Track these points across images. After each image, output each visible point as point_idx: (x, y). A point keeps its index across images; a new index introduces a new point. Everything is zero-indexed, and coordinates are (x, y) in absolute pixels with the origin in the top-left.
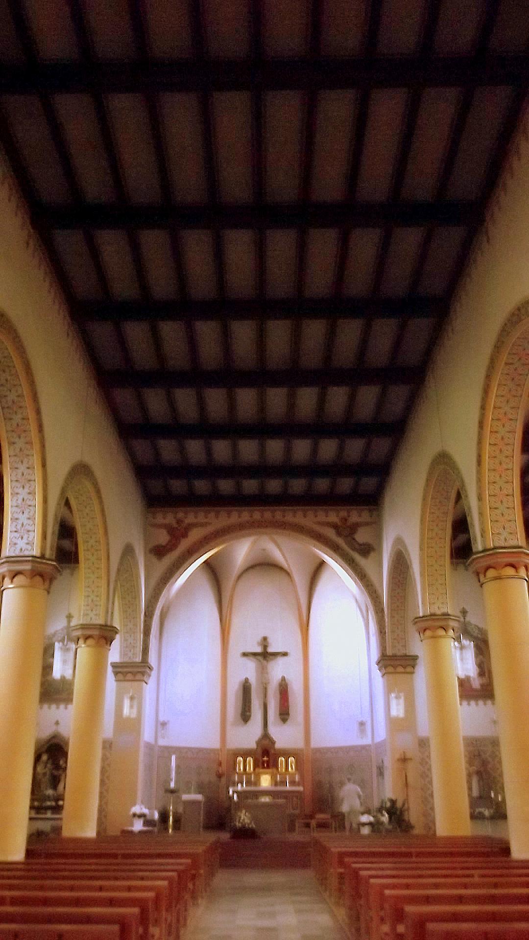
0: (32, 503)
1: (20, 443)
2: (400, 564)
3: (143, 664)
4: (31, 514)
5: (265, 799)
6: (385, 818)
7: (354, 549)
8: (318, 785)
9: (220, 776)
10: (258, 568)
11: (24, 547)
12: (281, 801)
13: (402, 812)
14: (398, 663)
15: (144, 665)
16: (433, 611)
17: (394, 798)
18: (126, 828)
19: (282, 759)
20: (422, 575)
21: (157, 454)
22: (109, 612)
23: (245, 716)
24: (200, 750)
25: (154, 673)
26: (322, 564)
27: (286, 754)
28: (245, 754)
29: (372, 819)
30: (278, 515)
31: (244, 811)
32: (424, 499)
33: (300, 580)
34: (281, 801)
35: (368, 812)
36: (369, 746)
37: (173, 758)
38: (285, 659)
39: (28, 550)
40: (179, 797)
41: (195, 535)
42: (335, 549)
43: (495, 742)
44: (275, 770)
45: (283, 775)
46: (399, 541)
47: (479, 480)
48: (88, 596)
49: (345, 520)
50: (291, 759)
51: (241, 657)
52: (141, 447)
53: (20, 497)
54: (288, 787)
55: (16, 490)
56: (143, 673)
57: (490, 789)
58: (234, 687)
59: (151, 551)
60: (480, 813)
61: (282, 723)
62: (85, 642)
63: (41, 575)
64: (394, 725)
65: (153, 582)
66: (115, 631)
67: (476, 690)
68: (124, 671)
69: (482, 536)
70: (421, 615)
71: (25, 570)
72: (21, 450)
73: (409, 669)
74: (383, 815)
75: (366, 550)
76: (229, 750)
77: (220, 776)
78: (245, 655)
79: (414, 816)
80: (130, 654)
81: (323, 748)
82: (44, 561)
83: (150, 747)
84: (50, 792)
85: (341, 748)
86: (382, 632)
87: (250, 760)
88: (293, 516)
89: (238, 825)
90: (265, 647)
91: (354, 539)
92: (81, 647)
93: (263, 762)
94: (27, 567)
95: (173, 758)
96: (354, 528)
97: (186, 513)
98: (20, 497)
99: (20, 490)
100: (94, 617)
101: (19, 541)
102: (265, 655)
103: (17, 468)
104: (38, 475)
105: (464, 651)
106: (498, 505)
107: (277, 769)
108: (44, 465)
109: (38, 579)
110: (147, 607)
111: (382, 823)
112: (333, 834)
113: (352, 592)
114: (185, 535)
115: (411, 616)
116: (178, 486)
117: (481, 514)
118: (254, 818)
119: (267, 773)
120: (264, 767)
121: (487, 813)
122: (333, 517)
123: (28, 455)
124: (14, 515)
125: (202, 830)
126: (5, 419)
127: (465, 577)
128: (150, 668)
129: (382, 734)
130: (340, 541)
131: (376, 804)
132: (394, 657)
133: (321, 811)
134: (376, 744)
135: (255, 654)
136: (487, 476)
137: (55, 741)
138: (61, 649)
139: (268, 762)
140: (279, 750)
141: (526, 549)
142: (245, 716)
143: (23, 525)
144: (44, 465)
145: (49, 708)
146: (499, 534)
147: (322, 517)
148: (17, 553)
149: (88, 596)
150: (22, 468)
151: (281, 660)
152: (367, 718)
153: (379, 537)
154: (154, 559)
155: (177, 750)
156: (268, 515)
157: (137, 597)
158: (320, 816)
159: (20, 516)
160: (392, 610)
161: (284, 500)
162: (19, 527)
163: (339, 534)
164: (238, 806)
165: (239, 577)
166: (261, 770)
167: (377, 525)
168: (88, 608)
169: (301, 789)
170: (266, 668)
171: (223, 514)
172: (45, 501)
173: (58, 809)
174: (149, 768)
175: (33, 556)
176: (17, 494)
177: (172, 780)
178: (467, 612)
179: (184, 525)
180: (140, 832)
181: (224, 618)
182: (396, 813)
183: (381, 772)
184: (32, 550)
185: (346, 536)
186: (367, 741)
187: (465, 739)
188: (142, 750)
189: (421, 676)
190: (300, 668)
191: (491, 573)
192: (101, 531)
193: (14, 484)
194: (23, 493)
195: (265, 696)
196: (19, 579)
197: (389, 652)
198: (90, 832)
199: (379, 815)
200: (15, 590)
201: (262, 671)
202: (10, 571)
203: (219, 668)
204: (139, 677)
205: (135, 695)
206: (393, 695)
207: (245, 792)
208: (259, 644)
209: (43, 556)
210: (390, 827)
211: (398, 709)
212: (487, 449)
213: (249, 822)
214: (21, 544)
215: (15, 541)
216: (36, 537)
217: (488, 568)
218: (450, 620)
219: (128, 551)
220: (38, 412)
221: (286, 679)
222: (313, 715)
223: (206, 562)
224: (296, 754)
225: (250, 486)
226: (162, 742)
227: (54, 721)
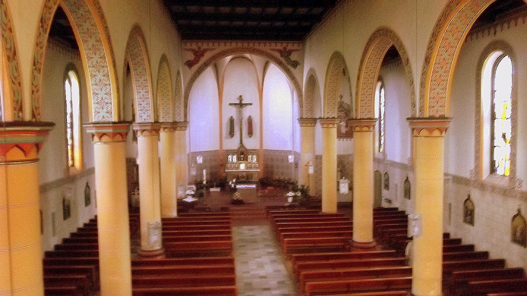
2: (312, 80)
10: (236, 59)
11: (146, 118)
23: (231, 133)
28: (233, 152)
32: (327, 75)
37: (204, 171)
38: (251, 106)
41: (208, 56)
49: (285, 48)
65: (188, 79)
78: (231, 104)
90: (241, 101)
91: (289, 59)
96: (290, 52)
97: (202, 43)
102: (241, 105)
114: (202, 55)
130: (282, 59)
142: (231, 133)
148: (143, 120)
150: (141, 80)
151: (248, 107)
154: (187, 68)
156: (246, 45)
160: (308, 97)
163: (282, 56)
171: (222, 44)
195: (241, 125)
201: (240, 113)
208: (237, 99)
214: (145, 116)
222: (264, 139)
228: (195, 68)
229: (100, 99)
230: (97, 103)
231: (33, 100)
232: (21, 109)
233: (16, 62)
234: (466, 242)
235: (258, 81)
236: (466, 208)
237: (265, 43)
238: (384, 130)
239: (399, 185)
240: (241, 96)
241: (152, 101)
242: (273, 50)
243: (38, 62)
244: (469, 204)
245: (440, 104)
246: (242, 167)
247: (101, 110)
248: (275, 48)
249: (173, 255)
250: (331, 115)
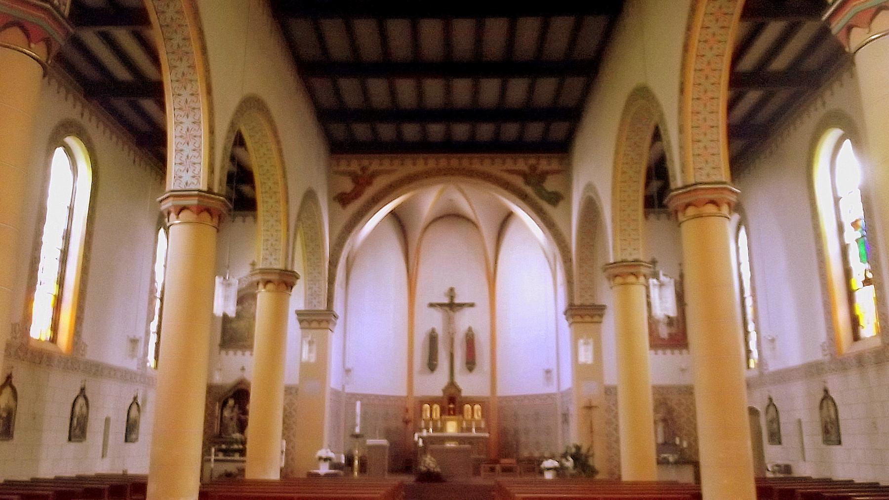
0: (198, 134)
1: (182, 67)
2: (591, 210)
3: (327, 312)
4: (197, 145)
5: (450, 445)
6: (569, 463)
7: (542, 197)
8: (503, 433)
9: (407, 422)
12: (467, 446)
13: (587, 457)
14: (587, 312)
15: (330, 312)
16: (624, 257)
17: (578, 444)
18: (311, 471)
19: (467, 407)
20: (613, 220)
22: (289, 256)
23: (432, 365)
24: (387, 397)
25: (339, 322)
26: (510, 215)
27: (472, 402)
28: (432, 401)
29: (556, 464)
30: (465, 163)
31: (429, 456)
33: (488, 232)
34: (467, 446)
35: (552, 457)
36: (554, 394)
37: (358, 404)
38: (471, 309)
39: (193, 183)
40: (365, 442)
41: (380, 183)
42: (524, 197)
43: (688, 391)
44: (461, 417)
45: (469, 423)
46: (590, 187)
47: (681, 110)
48: (267, 240)
50: (477, 407)
51: (428, 306)
52: (322, 86)
53: (185, 127)
54: (474, 433)
55: (180, 119)
56: (328, 321)
57: (674, 435)
58: (420, 339)
59: (335, 199)
60: (665, 458)
61: (469, 372)
62: (265, 287)
63: (208, 210)
64: (582, 372)
65: (339, 228)
66: (295, 276)
67: (663, 340)
68: (308, 319)
69: (683, 172)
70: (612, 261)
71: (192, 205)
72: (183, 74)
73: (596, 319)
74: (567, 460)
75: (555, 199)
76: (416, 398)
77: (407, 422)
78: (432, 305)
79: (597, 462)
81: (509, 397)
82: (213, 196)
83: (336, 393)
84: (237, 436)
85: (525, 397)
86: (569, 282)
87: (436, 407)
88: (478, 163)
89: (423, 468)
90: (452, 297)
92: (261, 291)
93: (449, 409)
94: (194, 202)
95: (358, 404)
96: (543, 176)
98: (185, 127)
99: (184, 120)
100: (273, 262)
101: (184, 174)
102: (452, 306)
103: (179, 95)
104: (202, 103)
105: (664, 288)
107: (463, 416)
108: (209, 92)
109: (205, 215)
110: (331, 255)
111: (567, 468)
112: (518, 479)
113: (540, 244)
114: (369, 183)
115: (600, 263)
116: (361, 131)
117: (682, 148)
118: (439, 463)
119: (452, 420)
120: (449, 414)
121: (671, 459)
122: (522, 164)
123: (191, 81)
124: (178, 146)
125: (387, 474)
126: (164, 39)
127: (660, 224)
128: (336, 317)
129: (567, 383)
130: (529, 190)
131: (561, 450)
132: (582, 307)
133: (506, 456)
134: (562, 393)
135: (441, 305)
136: (690, 105)
137: (240, 387)
138: (223, 284)
139: (454, 410)
140: (466, 398)
141: (729, 185)
142: (432, 365)
143: (188, 156)
144: (209, 92)
145: (235, 354)
147: (509, 164)
148: (183, 187)
149: (267, 240)
150: (186, 94)
151: (467, 311)
152: (553, 366)
153: (568, 185)
154: (337, 206)
155: (363, 397)
157: (319, 245)
158: (505, 461)
159: (185, 147)
160: (582, 260)
161: (472, 147)
162: (184, 159)
163: (527, 183)
164: (425, 450)
165: (426, 228)
166: (447, 417)
167: (566, 172)
168: (267, 252)
169: (487, 435)
170: (453, 318)
171: (409, 162)
172: (212, 132)
173: (242, 452)
174: (336, 415)
175: (199, 191)
176: (181, 123)
177: (356, 425)
178: (657, 262)
179: (369, 172)
180: (327, 475)
181: (411, 268)
182: (581, 459)
183: (566, 418)
184: (198, 184)
186: (552, 389)
187: (654, 387)
188: (328, 396)
189: (610, 324)
190: (487, 317)
191: (691, 211)
192: (279, 172)
193: (177, 112)
194: (187, 123)
196: (184, 215)
197: (577, 302)
198: (274, 475)
199: (564, 461)
200: (182, 226)
201: (449, 322)
202: (175, 206)
203: (405, 319)
204: (323, 325)
205: (315, 340)
206: (581, 341)
207: (429, 437)
208: (446, 295)
209: (210, 191)
210: (574, 472)
211: (586, 356)
212: (691, 76)
213: (434, 466)
214: (187, 177)
215: (180, 174)
216: (202, 170)
217: (688, 205)
218: (642, 267)
219: (310, 196)
220: (201, 32)
221: (473, 330)
222: (499, 376)
223: (393, 214)
224: (482, 402)
225: (436, 130)
226: (349, 389)
227: (240, 367)
235: (487, 260)
237: (493, 160)
238: (756, 320)
239: (804, 420)
240: (452, 290)
241: (207, 144)
246: (452, 428)
250: (630, 254)
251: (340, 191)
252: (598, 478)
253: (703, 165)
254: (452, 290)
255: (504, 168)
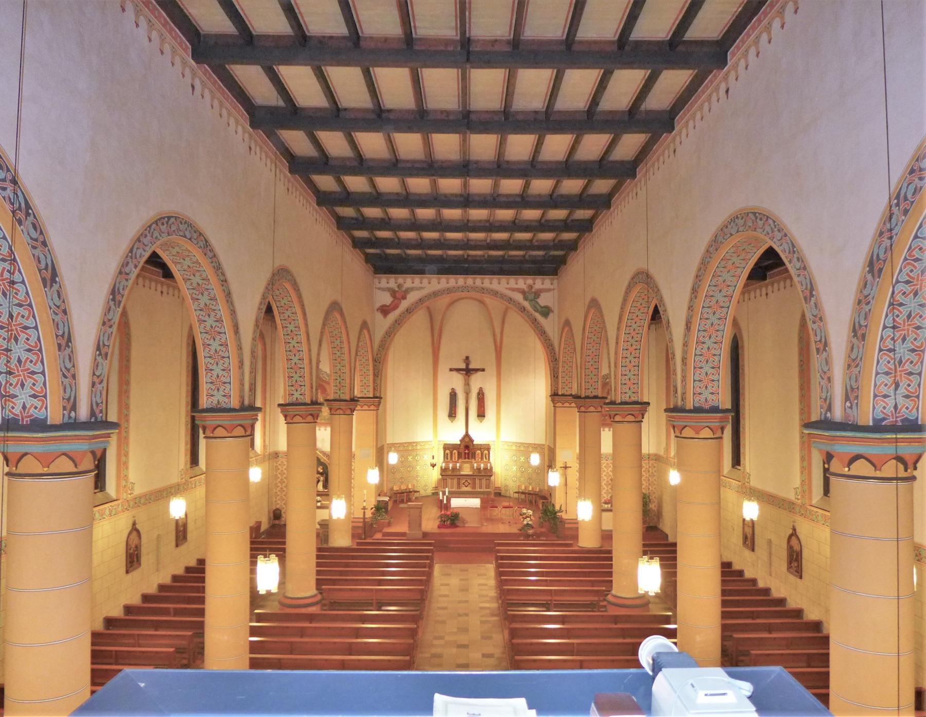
7: (537, 311)
16: (587, 394)
21: (374, 185)
80: (365, 391)
90: (467, 365)
91: (538, 303)
96: (537, 294)
101: (295, 393)
106: (627, 373)
114: (404, 298)
135: (458, 370)
139: (468, 454)
143: (296, 381)
146: (625, 393)
163: (526, 299)
185: (531, 300)
228: (392, 316)
229: (215, 376)
230: (211, 383)
231: (92, 393)
232: (74, 408)
233: (70, 349)
234: (793, 603)
236: (790, 548)
237: (499, 279)
240: (467, 358)
242: (513, 290)
243: (104, 345)
244: (794, 541)
245: (710, 390)
247: (215, 393)
248: (516, 286)
249: (334, 605)
251: (381, 304)
252: (614, 180)
253: (627, 390)
254: (467, 358)
255: (508, 286)
